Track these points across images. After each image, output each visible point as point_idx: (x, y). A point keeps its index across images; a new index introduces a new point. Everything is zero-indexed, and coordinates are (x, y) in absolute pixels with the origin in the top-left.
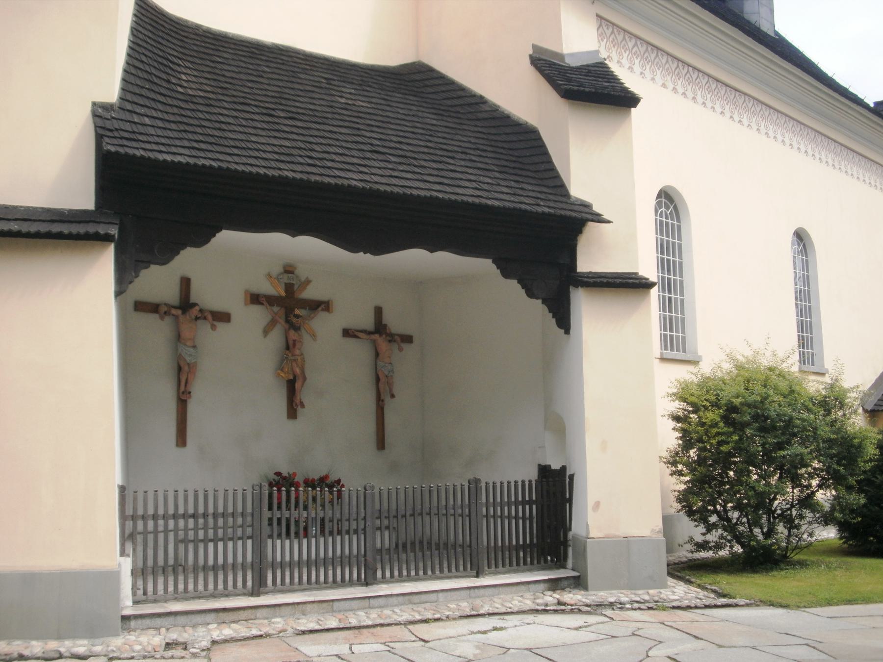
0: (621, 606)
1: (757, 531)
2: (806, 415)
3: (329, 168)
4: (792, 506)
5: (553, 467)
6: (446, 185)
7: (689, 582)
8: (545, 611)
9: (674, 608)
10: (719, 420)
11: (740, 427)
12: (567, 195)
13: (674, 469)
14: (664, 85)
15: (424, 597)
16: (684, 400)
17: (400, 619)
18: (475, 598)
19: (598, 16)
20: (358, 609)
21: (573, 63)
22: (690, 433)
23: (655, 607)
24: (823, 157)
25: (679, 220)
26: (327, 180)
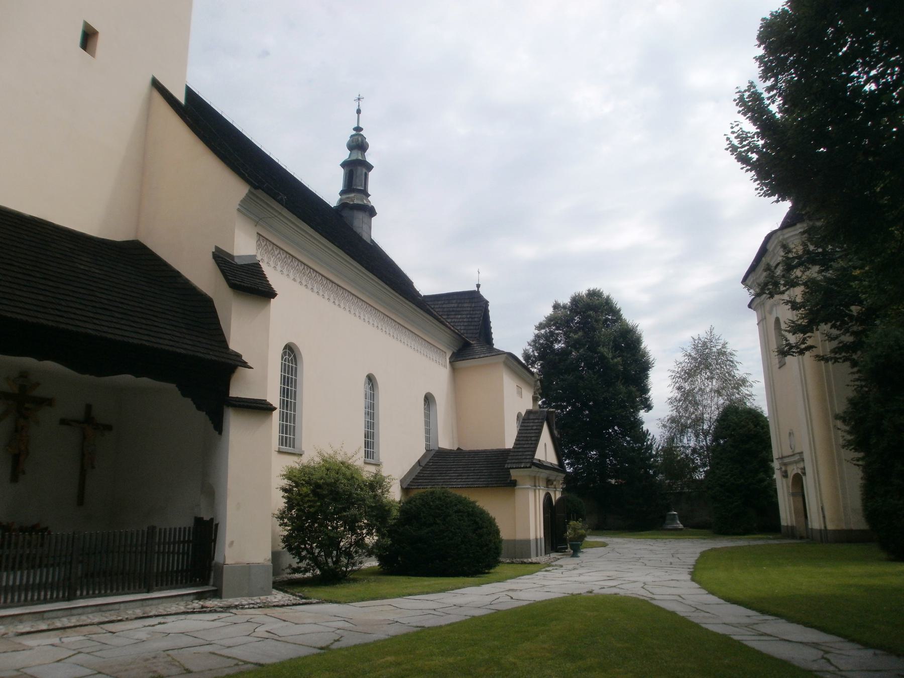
0: (242, 607)
1: (329, 560)
2: (359, 492)
3: (72, 319)
4: (351, 545)
5: (205, 519)
6: (153, 336)
7: (286, 592)
8: (193, 613)
9: (274, 606)
10: (309, 492)
11: (320, 497)
12: (226, 346)
13: (281, 521)
14: (294, 280)
15: (110, 607)
16: (289, 479)
17: (93, 621)
18: (146, 606)
19: (258, 233)
20: (63, 617)
21: (239, 262)
22: (292, 500)
23: (263, 606)
24: (387, 330)
25: (296, 364)
26: (70, 328)
